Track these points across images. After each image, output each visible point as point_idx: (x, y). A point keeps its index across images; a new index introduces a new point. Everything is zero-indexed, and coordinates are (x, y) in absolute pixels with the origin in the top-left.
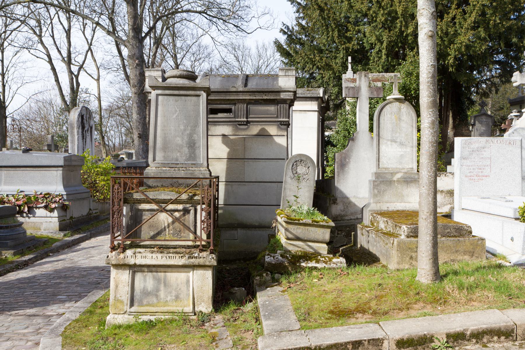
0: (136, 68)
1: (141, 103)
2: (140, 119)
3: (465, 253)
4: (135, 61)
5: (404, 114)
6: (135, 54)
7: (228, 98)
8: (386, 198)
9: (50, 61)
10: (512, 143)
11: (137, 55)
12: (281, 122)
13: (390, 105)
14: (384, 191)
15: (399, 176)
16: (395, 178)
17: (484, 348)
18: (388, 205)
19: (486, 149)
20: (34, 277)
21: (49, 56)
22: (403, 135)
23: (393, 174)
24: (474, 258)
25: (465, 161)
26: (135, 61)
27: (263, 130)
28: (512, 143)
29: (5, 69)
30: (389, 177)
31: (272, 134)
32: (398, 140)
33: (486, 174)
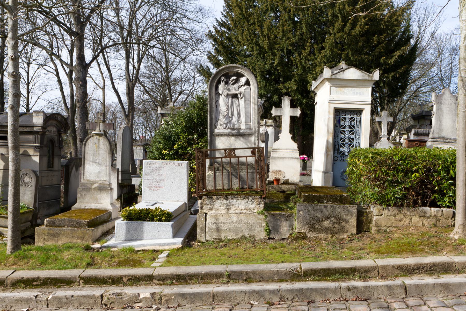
0: (80, 88)
1: (83, 115)
2: (82, 128)
3: (78, 238)
4: (79, 83)
5: (102, 144)
6: (79, 77)
7: (3, 130)
8: (86, 200)
9: (58, 75)
10: (180, 165)
11: (81, 78)
12: (36, 146)
13: (92, 138)
14: (85, 195)
15: (96, 185)
16: (93, 187)
17: (168, 309)
18: (86, 205)
19: (162, 169)
20: (404, 275)
21: (57, 70)
22: (101, 158)
23: (92, 184)
24: (84, 241)
25: (147, 176)
26: (79, 83)
27: (25, 151)
28: (180, 165)
29: (30, 78)
30: (89, 186)
31: (31, 154)
32: (97, 161)
33: (161, 186)
